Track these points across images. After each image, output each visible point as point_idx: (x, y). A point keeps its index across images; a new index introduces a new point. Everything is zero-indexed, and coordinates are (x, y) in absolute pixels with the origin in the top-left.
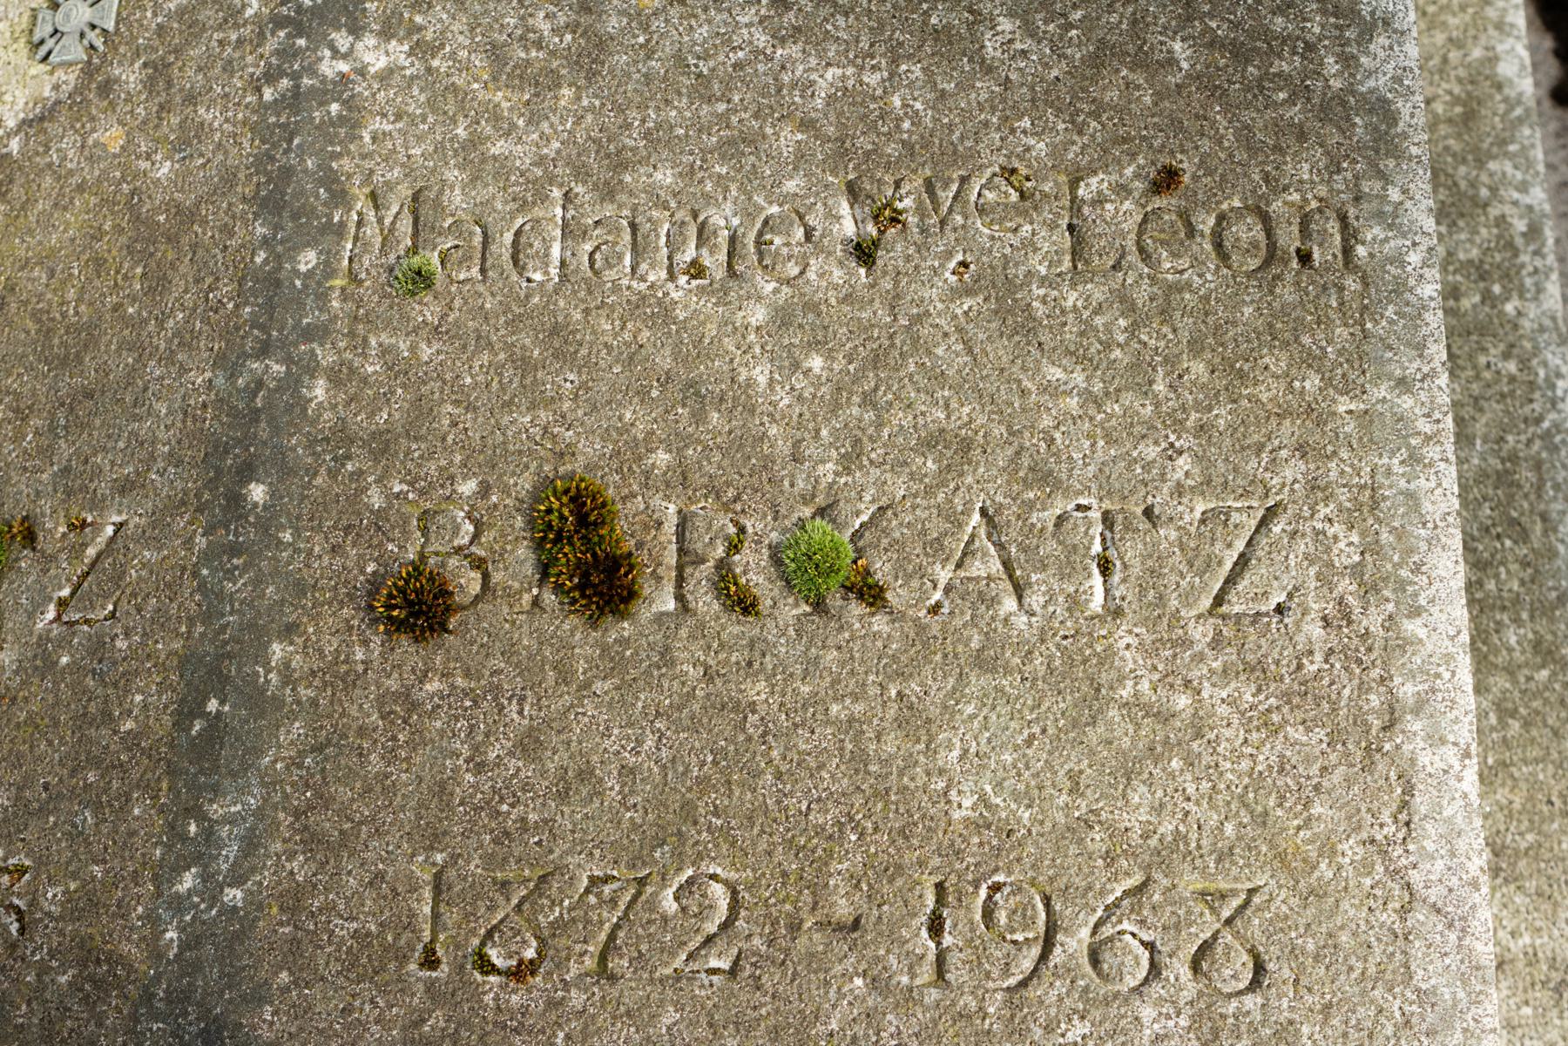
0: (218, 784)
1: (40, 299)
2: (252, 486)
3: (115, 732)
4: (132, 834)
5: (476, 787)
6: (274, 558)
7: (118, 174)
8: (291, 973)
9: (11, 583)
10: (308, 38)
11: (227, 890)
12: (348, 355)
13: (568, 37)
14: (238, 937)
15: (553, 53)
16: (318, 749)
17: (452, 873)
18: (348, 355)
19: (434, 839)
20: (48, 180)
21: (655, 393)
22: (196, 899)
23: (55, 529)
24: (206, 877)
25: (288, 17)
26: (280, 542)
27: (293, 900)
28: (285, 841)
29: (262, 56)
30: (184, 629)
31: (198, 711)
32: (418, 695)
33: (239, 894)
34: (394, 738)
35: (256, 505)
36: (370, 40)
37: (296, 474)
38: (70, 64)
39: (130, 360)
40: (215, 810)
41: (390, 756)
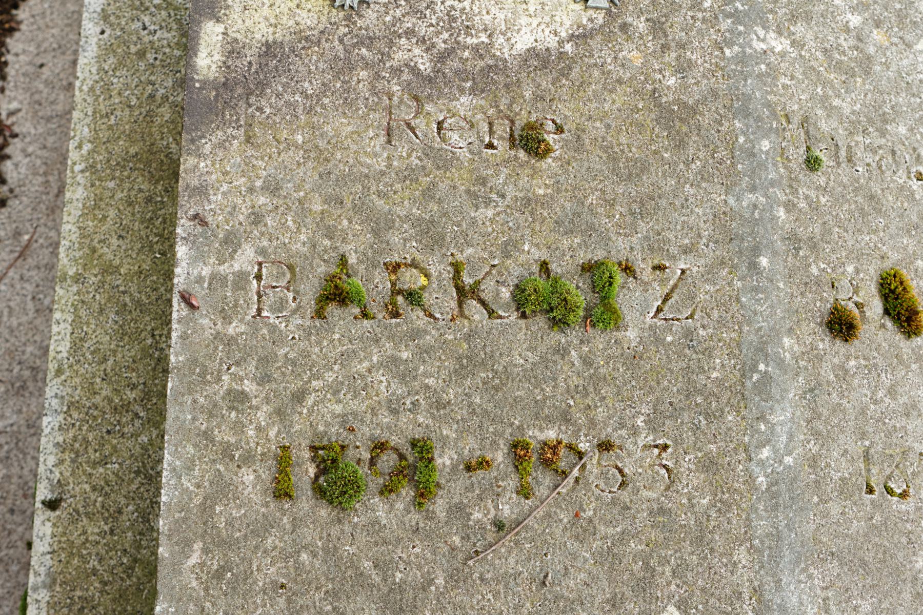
0: (772, 406)
1: (604, 140)
2: (761, 258)
3: (709, 378)
4: (730, 429)
5: (875, 411)
6: (777, 296)
7: (642, 78)
8: (818, 497)
9: (624, 296)
10: (745, 26)
11: (785, 457)
12: (791, 197)
13: (855, 52)
14: (794, 480)
15: (850, 59)
16: (812, 390)
17: (872, 451)
18: (791, 197)
19: (863, 436)
20: (596, 73)
21: (913, 233)
22: (772, 462)
23: (644, 269)
24: (776, 451)
25: (730, 13)
26: (778, 288)
27: (813, 462)
28: (805, 434)
29: (719, 31)
30: (737, 328)
31: (754, 369)
32: (847, 367)
33: (791, 460)
34: (841, 387)
35: (765, 268)
36: (773, 35)
37: (779, 255)
38: (602, 9)
39: (673, 183)
40: (773, 418)
41: (842, 396)
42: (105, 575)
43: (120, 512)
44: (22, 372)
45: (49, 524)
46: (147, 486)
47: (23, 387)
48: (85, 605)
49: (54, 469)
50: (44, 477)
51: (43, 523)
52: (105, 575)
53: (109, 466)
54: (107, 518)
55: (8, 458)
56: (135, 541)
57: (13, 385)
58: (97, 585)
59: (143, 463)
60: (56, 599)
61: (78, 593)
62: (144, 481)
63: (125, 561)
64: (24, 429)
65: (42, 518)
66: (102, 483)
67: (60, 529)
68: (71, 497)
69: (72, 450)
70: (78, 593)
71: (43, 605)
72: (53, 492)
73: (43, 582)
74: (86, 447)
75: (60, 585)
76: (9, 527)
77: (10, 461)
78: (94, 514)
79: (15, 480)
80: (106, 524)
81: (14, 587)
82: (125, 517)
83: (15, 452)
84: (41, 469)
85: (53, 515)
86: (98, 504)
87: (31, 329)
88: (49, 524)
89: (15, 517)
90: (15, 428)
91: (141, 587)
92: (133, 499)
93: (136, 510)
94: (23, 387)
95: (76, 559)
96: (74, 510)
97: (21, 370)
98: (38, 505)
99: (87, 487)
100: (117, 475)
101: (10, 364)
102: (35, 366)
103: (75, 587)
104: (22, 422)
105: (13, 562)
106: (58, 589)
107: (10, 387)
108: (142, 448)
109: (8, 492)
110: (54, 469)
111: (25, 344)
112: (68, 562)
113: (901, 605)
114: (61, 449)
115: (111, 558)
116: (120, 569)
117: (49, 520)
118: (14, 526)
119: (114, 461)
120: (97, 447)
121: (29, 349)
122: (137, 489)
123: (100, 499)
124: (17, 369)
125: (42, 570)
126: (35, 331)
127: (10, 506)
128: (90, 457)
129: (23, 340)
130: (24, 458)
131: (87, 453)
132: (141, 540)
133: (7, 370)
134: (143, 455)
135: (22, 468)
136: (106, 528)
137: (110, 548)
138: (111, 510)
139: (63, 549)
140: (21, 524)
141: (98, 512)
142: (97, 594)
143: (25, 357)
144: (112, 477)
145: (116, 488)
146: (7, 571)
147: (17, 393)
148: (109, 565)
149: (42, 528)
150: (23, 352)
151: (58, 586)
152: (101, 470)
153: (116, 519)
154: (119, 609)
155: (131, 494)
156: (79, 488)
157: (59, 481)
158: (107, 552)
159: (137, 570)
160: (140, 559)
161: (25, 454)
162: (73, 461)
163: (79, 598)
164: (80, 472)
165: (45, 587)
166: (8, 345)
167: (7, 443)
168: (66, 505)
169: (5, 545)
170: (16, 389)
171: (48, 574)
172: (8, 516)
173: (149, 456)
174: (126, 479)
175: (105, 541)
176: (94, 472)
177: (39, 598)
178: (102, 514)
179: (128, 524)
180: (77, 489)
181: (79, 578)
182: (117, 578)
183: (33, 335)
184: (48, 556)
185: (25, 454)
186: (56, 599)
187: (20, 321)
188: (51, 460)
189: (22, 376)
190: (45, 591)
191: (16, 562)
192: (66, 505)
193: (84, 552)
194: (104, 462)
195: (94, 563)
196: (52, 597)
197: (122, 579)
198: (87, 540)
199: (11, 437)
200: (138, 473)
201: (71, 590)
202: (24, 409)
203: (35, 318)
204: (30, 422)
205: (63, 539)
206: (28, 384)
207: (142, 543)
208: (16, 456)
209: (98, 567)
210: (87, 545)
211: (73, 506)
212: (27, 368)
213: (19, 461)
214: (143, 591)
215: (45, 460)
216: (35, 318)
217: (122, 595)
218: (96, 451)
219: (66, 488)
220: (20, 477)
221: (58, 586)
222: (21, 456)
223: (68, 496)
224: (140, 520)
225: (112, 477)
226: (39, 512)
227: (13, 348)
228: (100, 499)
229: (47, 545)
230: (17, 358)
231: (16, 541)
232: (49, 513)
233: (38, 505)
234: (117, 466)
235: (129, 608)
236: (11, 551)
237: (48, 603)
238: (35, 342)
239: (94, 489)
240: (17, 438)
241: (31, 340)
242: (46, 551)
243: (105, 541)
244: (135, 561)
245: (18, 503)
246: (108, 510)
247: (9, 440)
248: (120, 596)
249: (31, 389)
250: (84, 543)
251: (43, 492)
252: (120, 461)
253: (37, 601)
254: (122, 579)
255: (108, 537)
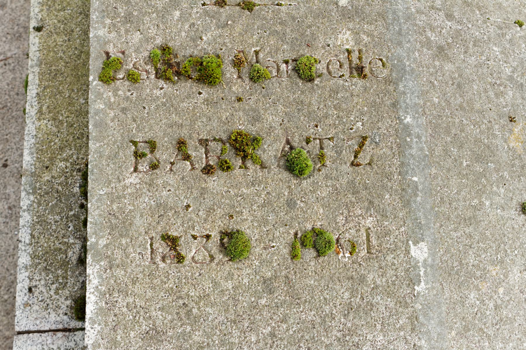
42: (67, 59)
43: (72, 31)
44: (19, 29)
45: (37, 38)
46: (85, 19)
47: (20, 36)
48: (57, 73)
49: (38, 14)
50: (34, 17)
51: (34, 38)
52: (67, 59)
53: (66, 11)
54: (66, 34)
55: (14, 69)
56: (81, 44)
57: (14, 35)
58: (63, 64)
59: (83, 9)
60: (43, 71)
61: (54, 68)
62: (84, 17)
63: (76, 53)
64: (21, 56)
65: (34, 35)
66: (63, 19)
67: (43, 40)
68: (48, 26)
69: (47, 5)
70: (54, 68)
71: (36, 74)
72: (38, 23)
73: (36, 64)
74: (54, 3)
75: (45, 65)
76: (16, 101)
77: (15, 71)
78: (60, 33)
79: (18, 79)
80: (66, 37)
81: (21, 129)
82: (75, 33)
83: (17, 66)
84: (32, 14)
85: (39, 34)
86: (61, 28)
87: (23, 9)
88: (37, 38)
89: (19, 97)
90: (17, 55)
91: (85, 64)
92: (79, 25)
93: (81, 30)
94: (20, 36)
95: (52, 53)
96: (49, 31)
97: (18, 28)
98: (31, 30)
99: (56, 21)
100: (70, 15)
101: (13, 26)
102: (26, 26)
103: (52, 65)
104: (20, 52)
105: (19, 117)
106: (43, 66)
107: (13, 36)
108: (82, 2)
109: (15, 85)
110: (38, 14)
111: (20, 16)
112: (48, 55)
113: (456, 5)
114: (42, 5)
115: (69, 52)
116: (74, 56)
117: (37, 36)
118: (19, 101)
119: (69, 9)
120: (59, 3)
121: (22, 18)
122: (81, 20)
123: (62, 26)
124: (16, 28)
125: (35, 59)
126: (24, 10)
127: (16, 92)
128: (56, 8)
129: (19, 14)
130: (22, 70)
131: (55, 6)
132: (84, 43)
133: (11, 28)
134: (83, 6)
135: (22, 74)
136: (66, 39)
137: (68, 47)
138: (68, 31)
139: (45, 49)
140: (23, 100)
141: (62, 32)
142: (63, 68)
143: (20, 22)
144: (68, 16)
145: (70, 20)
146: (17, 122)
147: (17, 39)
148: (68, 55)
149: (34, 40)
150: (19, 20)
151: (43, 65)
152: (62, 13)
153: (71, 35)
154: (74, 74)
155: (78, 23)
156: (51, 22)
157: (41, 19)
158: (67, 49)
159: (82, 56)
160: (84, 51)
161: (23, 67)
162: (48, 10)
163: (54, 70)
164: (52, 15)
165: (36, 65)
166: (11, 17)
167: (13, 63)
168: (45, 30)
169: (15, 110)
170: (16, 37)
171: (38, 60)
172: (16, 96)
173: (86, 6)
174: (75, 16)
175: (66, 44)
176: (59, 14)
177: (34, 71)
178: (64, 32)
179: (77, 36)
180: (50, 22)
181: (53, 61)
182: (73, 60)
183: (24, 12)
184: (38, 52)
185: (23, 67)
186: (43, 71)
187: (17, 5)
188: (37, 10)
189: (19, 31)
190: (37, 68)
191: (21, 117)
192: (45, 30)
193: (56, 50)
194: (63, 9)
195: (61, 54)
196: (40, 70)
197: (75, 61)
198: (57, 44)
199: (15, 60)
200: (81, 13)
201: (50, 67)
202: (21, 47)
203: (24, 4)
204: (24, 52)
205: (45, 44)
206: (23, 35)
207: (85, 44)
208: (18, 68)
209: (63, 56)
210: (57, 46)
211: (49, 29)
212: (22, 27)
213: (20, 71)
214: (86, 65)
215: (34, 10)
216: (24, 4)
217: (76, 67)
218: (59, 5)
219: (45, 22)
220: (21, 78)
221: (43, 65)
222: (21, 68)
223: (46, 25)
224: (83, 34)
225: (68, 16)
226: (32, 33)
227: (14, 18)
228: (62, 26)
229: (37, 47)
230: (16, 23)
231: (20, 108)
232: (37, 33)
233: (31, 30)
234: (70, 11)
235: (79, 73)
236: (18, 113)
237: (39, 73)
238: (25, 15)
239: (59, 22)
240: (18, 60)
241: (23, 14)
242: (36, 50)
243: (66, 44)
244: (82, 52)
245: (20, 90)
246: (66, 31)
247: (14, 61)
248: (75, 68)
249: (24, 37)
250: (55, 46)
251: (33, 24)
252: (71, 9)
253: (33, 72)
254: (75, 61)
255: (67, 42)
